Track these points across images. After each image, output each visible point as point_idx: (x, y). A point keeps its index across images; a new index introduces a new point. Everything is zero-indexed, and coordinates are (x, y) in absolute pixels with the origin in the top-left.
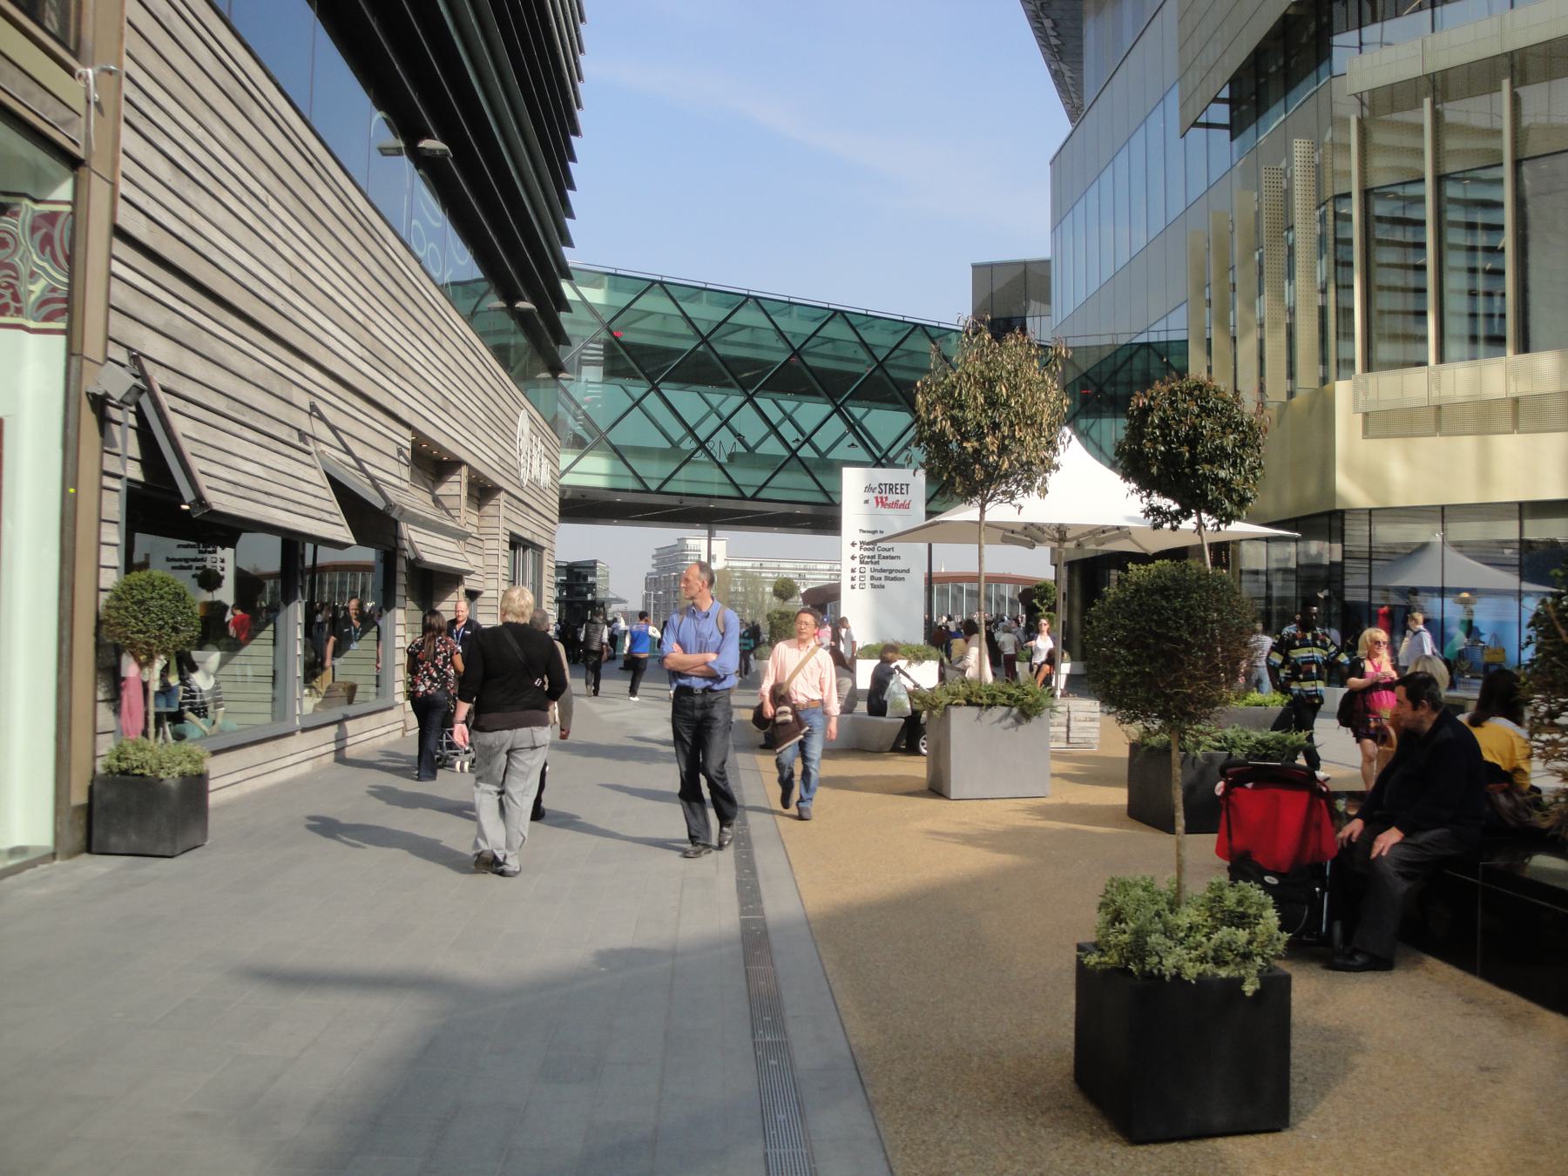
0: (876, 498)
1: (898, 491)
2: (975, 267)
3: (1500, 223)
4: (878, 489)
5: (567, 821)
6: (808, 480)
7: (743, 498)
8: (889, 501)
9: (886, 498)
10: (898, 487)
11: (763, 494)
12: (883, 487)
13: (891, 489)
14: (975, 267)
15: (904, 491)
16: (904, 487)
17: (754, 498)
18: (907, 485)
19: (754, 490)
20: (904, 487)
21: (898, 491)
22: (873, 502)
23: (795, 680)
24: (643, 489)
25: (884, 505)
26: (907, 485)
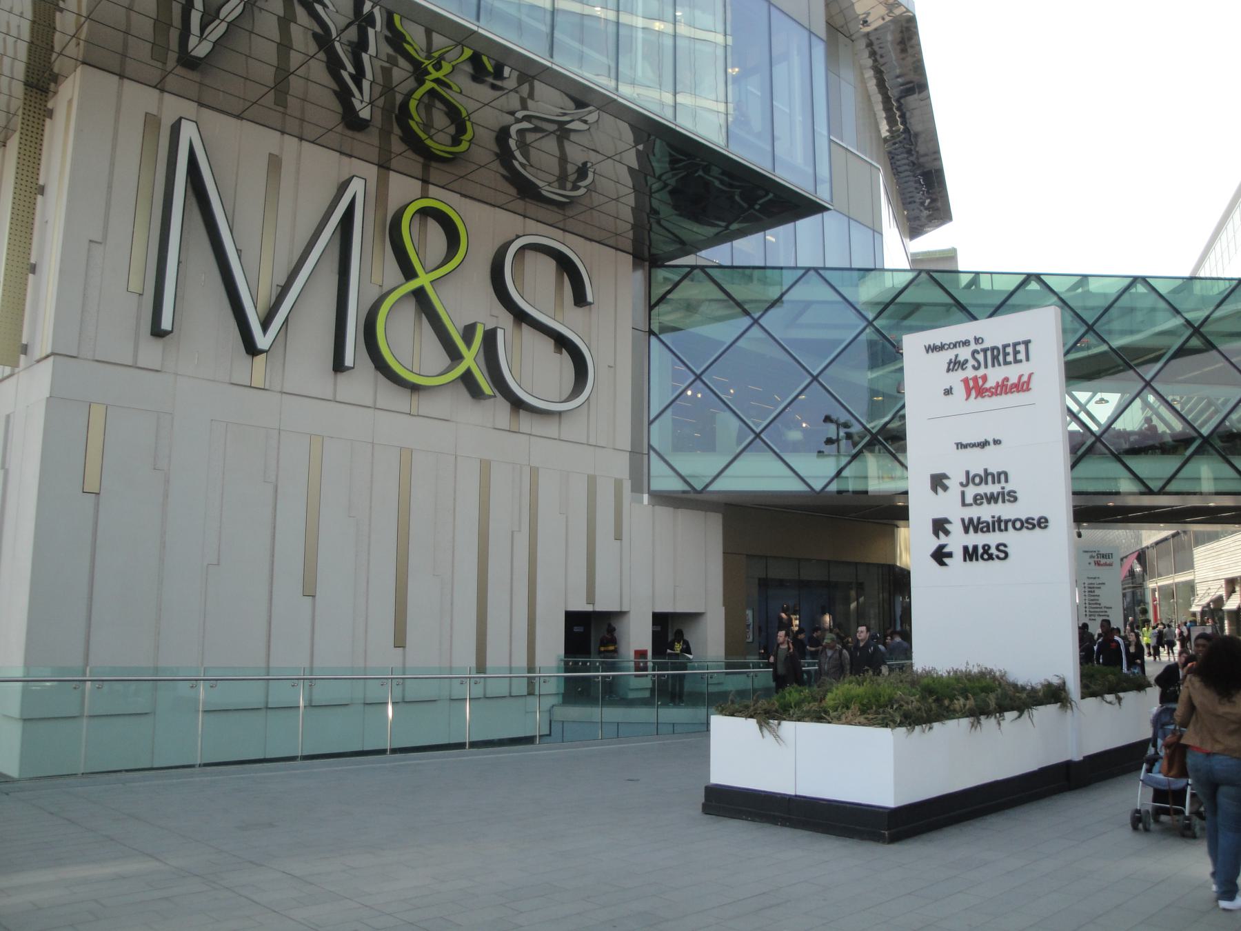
0: (966, 381)
1: (1010, 358)
2: (954, 250)
3: (633, 494)
4: (972, 362)
5: (219, 560)
6: (1227, 468)
7: (1150, 492)
8: (990, 383)
9: (985, 378)
10: (1010, 350)
11: (1172, 487)
12: (980, 357)
13: (995, 358)
14: (954, 250)
15: (1022, 356)
16: (1021, 348)
17: (1162, 492)
18: (1027, 343)
19: (1160, 484)
20: (1021, 348)
21: (1010, 358)
22: (960, 390)
23: (653, 204)
24: (1147, 491)
25: (981, 392)
26: (1027, 343)
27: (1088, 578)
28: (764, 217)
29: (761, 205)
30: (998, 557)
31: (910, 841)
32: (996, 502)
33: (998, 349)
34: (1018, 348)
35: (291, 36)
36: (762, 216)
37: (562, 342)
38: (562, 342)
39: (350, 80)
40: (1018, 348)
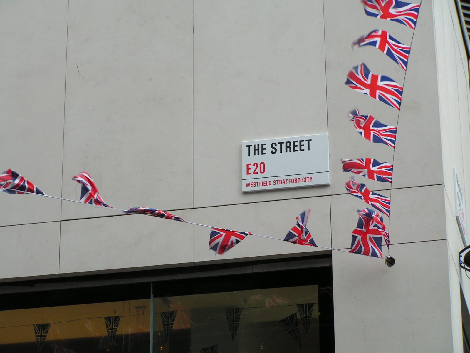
1: (297, 148)
10: (297, 144)
21: (297, 148)
26: (308, 141)
27: (249, 155)
28: (309, 233)
29: (309, 241)
30: (275, 181)
31: (463, 332)
32: (360, 225)
33: (290, 143)
34: (302, 143)
35: (443, 175)
36: (308, 234)
37: (241, 309)
38: (241, 309)
39: (386, 142)
40: (302, 143)
